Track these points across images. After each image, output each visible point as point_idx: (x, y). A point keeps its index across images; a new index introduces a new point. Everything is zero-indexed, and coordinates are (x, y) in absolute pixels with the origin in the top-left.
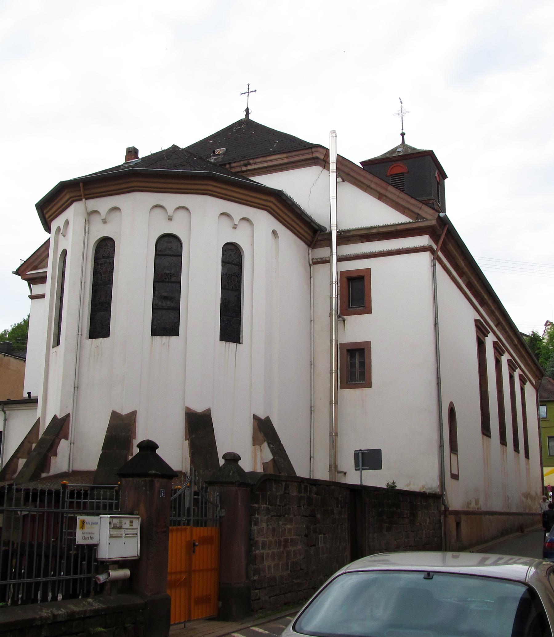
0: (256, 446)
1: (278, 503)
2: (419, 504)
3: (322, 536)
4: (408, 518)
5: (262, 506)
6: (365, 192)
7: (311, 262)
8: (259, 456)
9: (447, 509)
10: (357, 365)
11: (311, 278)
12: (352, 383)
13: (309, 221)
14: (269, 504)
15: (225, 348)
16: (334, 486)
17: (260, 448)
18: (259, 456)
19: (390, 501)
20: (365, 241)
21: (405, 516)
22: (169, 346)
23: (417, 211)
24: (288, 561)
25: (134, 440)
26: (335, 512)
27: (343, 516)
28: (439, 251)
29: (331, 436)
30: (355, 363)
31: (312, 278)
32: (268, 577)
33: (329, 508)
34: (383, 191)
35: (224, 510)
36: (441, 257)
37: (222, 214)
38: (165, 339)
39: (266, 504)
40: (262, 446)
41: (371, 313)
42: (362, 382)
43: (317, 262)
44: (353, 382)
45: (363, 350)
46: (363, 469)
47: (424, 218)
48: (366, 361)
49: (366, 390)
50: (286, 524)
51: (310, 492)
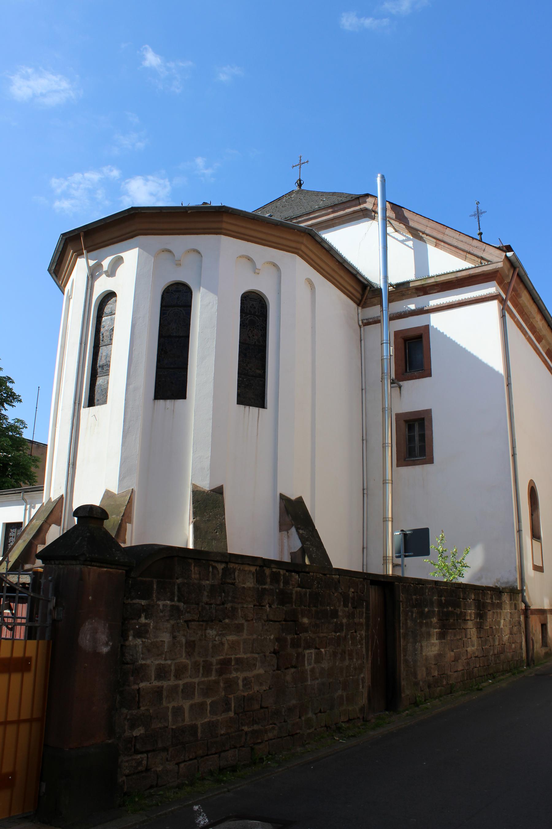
0: (283, 532)
1: (205, 599)
2: (489, 601)
3: (313, 651)
4: (472, 620)
5: (161, 603)
6: (420, 240)
7: (360, 323)
8: (286, 544)
9: (527, 607)
10: (417, 438)
11: (361, 341)
12: (411, 459)
13: (355, 272)
14: (179, 601)
15: (244, 414)
16: (339, 575)
17: (288, 535)
18: (286, 544)
19: (443, 598)
20: (422, 294)
21: (468, 618)
22: (173, 411)
23: (480, 254)
24: (231, 696)
25: (127, 524)
26: (340, 614)
27: (356, 620)
28: (509, 301)
29: (385, 522)
30: (414, 436)
31: (362, 341)
32: (172, 729)
33: (328, 608)
34: (440, 236)
35: (61, 608)
36: (512, 309)
37: (242, 257)
38: (169, 403)
39: (172, 600)
40: (290, 531)
41: (431, 376)
42: (422, 458)
43: (367, 323)
44: (412, 458)
45: (423, 419)
46: (406, 556)
47: (488, 261)
48: (427, 432)
49: (427, 467)
50: (223, 635)
51: (286, 583)
